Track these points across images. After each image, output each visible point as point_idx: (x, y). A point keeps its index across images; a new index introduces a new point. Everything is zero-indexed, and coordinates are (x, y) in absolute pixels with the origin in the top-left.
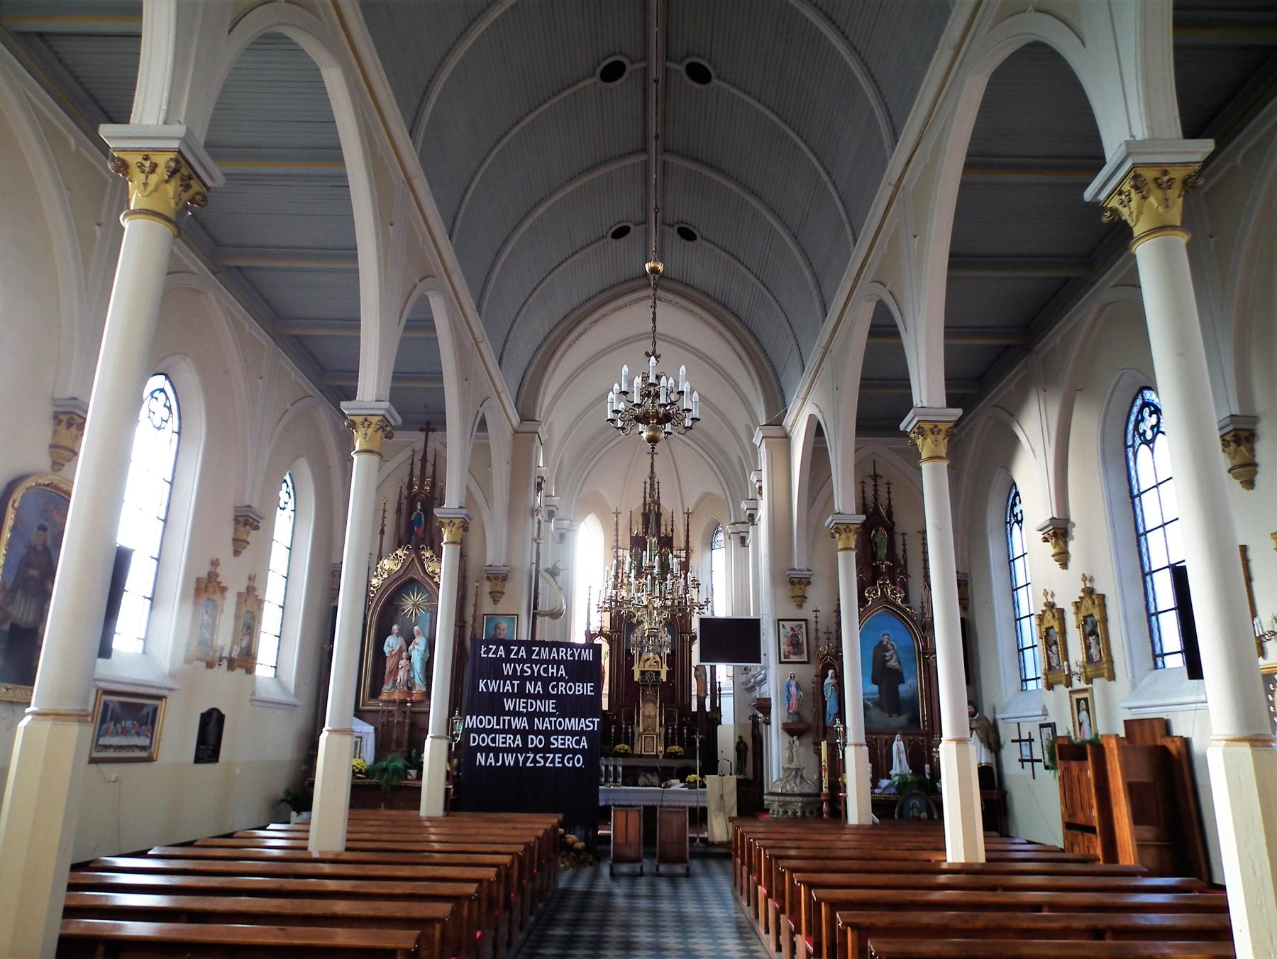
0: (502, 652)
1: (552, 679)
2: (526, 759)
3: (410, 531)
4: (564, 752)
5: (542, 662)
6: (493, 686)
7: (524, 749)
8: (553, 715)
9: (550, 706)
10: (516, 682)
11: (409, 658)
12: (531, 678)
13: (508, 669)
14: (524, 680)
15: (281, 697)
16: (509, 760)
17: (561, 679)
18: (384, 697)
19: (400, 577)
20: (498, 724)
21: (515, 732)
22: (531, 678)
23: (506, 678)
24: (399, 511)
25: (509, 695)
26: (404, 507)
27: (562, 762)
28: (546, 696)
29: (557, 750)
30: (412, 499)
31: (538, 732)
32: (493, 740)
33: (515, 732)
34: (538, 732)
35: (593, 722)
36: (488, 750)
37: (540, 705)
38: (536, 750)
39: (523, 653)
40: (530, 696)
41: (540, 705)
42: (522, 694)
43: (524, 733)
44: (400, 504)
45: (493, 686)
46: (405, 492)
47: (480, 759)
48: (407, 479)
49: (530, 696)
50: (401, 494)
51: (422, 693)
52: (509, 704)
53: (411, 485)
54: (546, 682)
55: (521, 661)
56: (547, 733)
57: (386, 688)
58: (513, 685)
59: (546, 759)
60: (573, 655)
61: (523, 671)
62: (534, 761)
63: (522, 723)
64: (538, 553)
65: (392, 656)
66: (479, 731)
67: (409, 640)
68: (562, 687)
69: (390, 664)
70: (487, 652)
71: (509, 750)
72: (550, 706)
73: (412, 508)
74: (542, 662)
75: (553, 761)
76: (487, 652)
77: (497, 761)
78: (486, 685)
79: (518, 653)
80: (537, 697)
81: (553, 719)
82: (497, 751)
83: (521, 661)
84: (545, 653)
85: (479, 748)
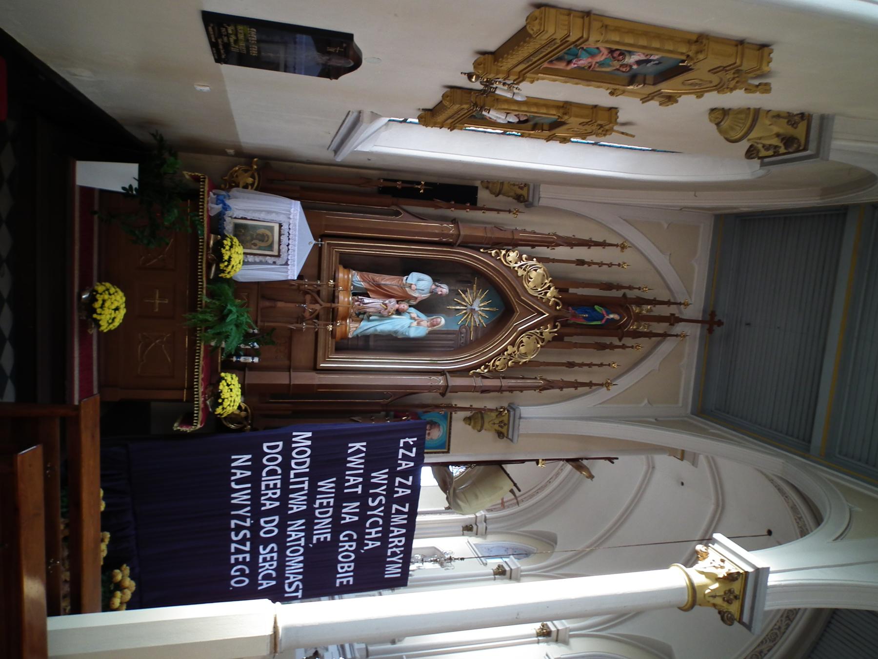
0: (404, 465)
1: (362, 535)
2: (243, 518)
3: (586, 304)
4: (254, 565)
5: (387, 517)
6: (355, 462)
7: (257, 512)
8: (308, 538)
9: (322, 532)
10: (359, 490)
11: (399, 312)
12: (364, 507)
13: (380, 477)
14: (363, 498)
15: (498, 315)
16: (241, 497)
17: (361, 543)
18: (342, 275)
19: (518, 295)
20: (297, 475)
21: (284, 499)
22: (364, 507)
23: (366, 476)
24: (609, 286)
25: (340, 484)
26: (614, 293)
27: (237, 562)
28: (337, 527)
29: (254, 553)
30: (622, 305)
31: (282, 527)
32: (272, 473)
33: (284, 499)
34: (282, 527)
35: (296, 590)
36: (256, 467)
37: (323, 523)
38: (255, 528)
39: (401, 492)
40: (338, 508)
41: (323, 523)
42: (341, 498)
43: (282, 511)
44: (619, 287)
45: (355, 462)
46: (631, 294)
47: (243, 459)
48: (649, 295)
49: (338, 508)
50: (630, 288)
51: (345, 337)
52: (327, 485)
53: (640, 301)
54: (359, 527)
55: (390, 490)
56: (281, 540)
57: (357, 279)
58: (355, 486)
59: (242, 542)
60: (394, 554)
61: (375, 496)
62: (239, 529)
63: (298, 503)
64: (523, 461)
65: (402, 287)
66: (287, 453)
67: (427, 307)
68: (348, 547)
69: (388, 281)
70: (408, 447)
71: (256, 494)
72: (322, 532)
73: (609, 304)
74: (387, 517)
75: (239, 552)
76: (408, 447)
77: (238, 482)
78: (359, 451)
79: (402, 485)
80: (337, 517)
81: (302, 542)
82: (255, 480)
83: (390, 490)
84: (398, 520)
85: (258, 455)
